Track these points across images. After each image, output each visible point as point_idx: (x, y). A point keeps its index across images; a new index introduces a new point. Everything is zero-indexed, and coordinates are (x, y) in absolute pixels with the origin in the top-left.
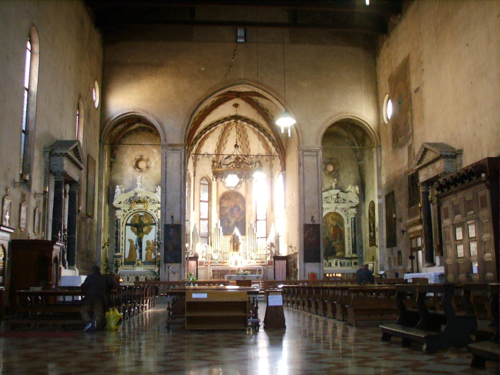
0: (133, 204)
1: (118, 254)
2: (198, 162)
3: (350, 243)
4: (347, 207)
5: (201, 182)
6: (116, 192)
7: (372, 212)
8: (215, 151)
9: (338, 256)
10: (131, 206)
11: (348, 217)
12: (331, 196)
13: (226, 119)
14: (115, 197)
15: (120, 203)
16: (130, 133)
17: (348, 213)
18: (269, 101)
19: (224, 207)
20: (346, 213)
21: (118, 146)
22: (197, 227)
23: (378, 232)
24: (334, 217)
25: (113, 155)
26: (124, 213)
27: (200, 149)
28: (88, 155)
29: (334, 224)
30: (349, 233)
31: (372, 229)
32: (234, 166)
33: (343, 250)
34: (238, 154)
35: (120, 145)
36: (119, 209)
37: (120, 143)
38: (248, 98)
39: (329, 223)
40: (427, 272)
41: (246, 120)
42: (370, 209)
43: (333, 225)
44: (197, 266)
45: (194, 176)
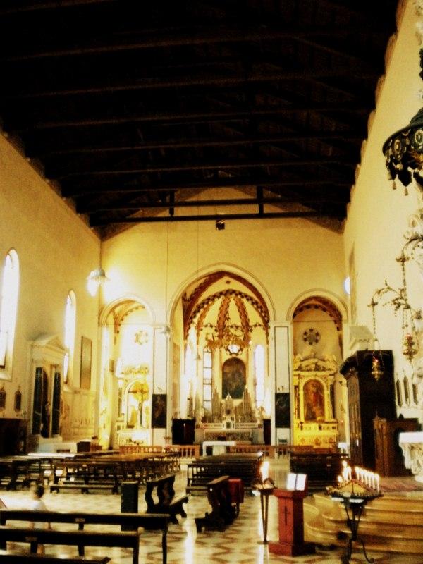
1: (120, 419)
16: (131, 311)
24: (315, 384)
28: (82, 337)
40: (228, 448)
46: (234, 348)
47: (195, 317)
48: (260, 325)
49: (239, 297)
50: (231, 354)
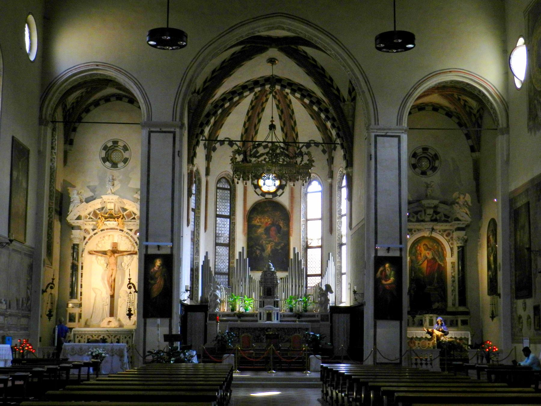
0: (99, 221)
2: (213, 154)
3: (455, 287)
4: (451, 228)
5: (218, 186)
6: (72, 200)
7: (493, 237)
8: (242, 136)
9: (436, 309)
10: (97, 223)
11: (452, 244)
12: (425, 210)
13: (256, 83)
14: (70, 209)
15: (79, 218)
16: (96, 104)
17: (452, 238)
18: (320, 52)
19: (255, 226)
20: (449, 238)
21: (77, 125)
22: (211, 257)
23: (501, 272)
25: (69, 142)
26: (133, 231)
27: (216, 131)
29: (430, 256)
30: (454, 271)
31: (493, 266)
32: (267, 160)
33: (444, 298)
34: (274, 140)
35: (81, 124)
36: (79, 228)
37: (80, 120)
38: (291, 47)
39: (421, 254)
41: (290, 84)
42: (490, 232)
43: (426, 258)
44: (206, 321)
45: (207, 173)
46: (269, 184)
47: (208, 123)
48: (317, 144)
49: (278, 87)
50: (264, 194)
